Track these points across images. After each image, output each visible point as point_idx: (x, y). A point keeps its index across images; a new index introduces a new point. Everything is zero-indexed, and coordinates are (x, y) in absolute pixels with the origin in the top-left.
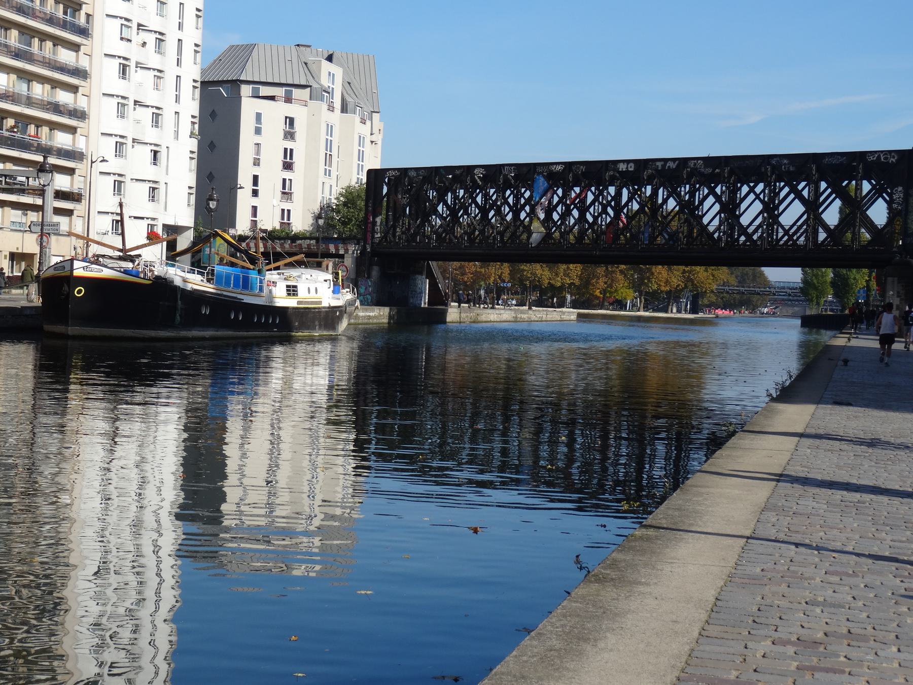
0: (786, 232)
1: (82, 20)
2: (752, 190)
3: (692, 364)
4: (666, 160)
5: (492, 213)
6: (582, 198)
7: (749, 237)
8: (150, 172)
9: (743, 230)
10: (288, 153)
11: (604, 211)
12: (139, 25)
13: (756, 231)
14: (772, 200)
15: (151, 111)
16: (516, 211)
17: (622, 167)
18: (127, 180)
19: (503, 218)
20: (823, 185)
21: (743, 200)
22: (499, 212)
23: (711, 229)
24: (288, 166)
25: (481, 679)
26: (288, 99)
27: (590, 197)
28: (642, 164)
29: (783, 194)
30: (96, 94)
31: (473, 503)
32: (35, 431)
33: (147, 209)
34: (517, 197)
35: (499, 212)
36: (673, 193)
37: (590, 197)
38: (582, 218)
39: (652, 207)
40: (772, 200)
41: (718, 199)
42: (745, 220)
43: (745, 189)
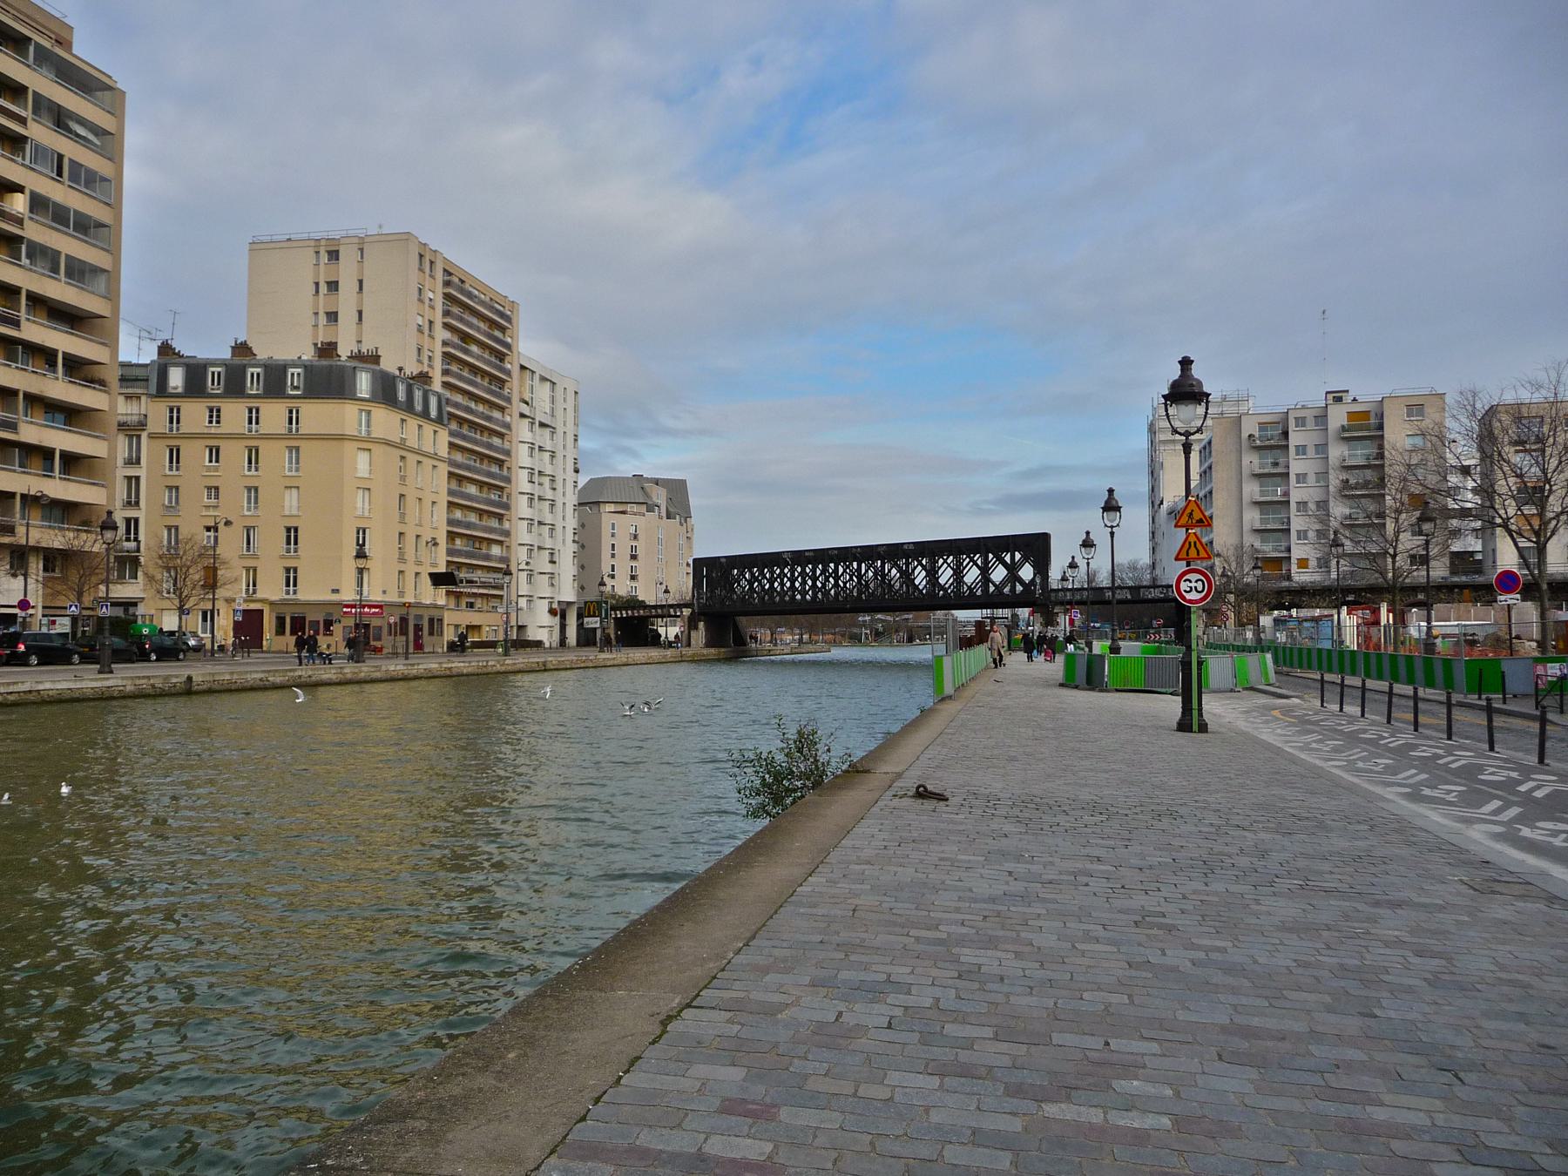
0: (969, 588)
1: (505, 472)
2: (945, 561)
5: (767, 587)
7: (945, 590)
8: (548, 568)
9: (942, 588)
11: (851, 579)
12: (540, 447)
13: (950, 587)
14: (958, 567)
16: (793, 580)
18: (535, 573)
19: (763, 587)
20: (991, 556)
21: (939, 568)
22: (760, 582)
23: (921, 587)
24: (634, 557)
27: (841, 570)
29: (965, 564)
30: (514, 519)
31: (38, 27)
34: (772, 572)
35: (760, 582)
36: (895, 565)
38: (836, 585)
40: (958, 567)
41: (924, 567)
42: (942, 581)
43: (941, 561)
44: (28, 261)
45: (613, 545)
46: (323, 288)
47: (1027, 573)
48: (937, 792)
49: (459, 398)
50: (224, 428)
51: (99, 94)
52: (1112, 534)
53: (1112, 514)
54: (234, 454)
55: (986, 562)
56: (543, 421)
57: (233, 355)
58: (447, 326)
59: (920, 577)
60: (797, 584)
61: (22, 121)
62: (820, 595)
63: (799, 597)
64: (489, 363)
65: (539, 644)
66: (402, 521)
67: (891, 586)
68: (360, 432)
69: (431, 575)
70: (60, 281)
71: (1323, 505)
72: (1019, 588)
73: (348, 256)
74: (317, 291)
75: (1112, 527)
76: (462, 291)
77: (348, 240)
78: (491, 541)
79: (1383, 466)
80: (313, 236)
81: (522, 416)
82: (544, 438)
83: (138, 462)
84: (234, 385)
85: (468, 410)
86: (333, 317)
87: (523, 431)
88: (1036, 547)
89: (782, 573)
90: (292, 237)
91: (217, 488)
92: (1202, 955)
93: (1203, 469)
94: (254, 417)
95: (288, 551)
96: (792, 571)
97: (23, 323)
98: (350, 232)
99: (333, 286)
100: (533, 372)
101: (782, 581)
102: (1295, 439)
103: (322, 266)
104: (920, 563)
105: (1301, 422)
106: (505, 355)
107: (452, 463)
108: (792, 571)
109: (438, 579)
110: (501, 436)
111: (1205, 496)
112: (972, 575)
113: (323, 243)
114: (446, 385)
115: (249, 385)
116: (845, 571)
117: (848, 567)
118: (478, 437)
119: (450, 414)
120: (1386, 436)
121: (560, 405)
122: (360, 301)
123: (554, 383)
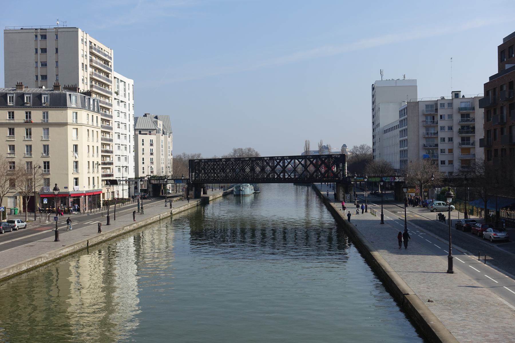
4: (278, 157)
10: (152, 150)
17: (266, 159)
24: (152, 154)
46: (39, 51)
48: (128, 194)
54: (21, 132)
56: (122, 100)
58: (91, 66)
73: (51, 37)
79: (475, 159)
81: (115, 99)
82: (121, 107)
86: (44, 64)
94: (28, 115)
95: (45, 171)
98: (51, 27)
99: (44, 51)
100: (118, 79)
102: (440, 112)
103: (39, 42)
105: (442, 105)
106: (109, 74)
113: (39, 31)
115: (43, 102)
119: (100, 106)
120: (476, 147)
123: (125, 82)
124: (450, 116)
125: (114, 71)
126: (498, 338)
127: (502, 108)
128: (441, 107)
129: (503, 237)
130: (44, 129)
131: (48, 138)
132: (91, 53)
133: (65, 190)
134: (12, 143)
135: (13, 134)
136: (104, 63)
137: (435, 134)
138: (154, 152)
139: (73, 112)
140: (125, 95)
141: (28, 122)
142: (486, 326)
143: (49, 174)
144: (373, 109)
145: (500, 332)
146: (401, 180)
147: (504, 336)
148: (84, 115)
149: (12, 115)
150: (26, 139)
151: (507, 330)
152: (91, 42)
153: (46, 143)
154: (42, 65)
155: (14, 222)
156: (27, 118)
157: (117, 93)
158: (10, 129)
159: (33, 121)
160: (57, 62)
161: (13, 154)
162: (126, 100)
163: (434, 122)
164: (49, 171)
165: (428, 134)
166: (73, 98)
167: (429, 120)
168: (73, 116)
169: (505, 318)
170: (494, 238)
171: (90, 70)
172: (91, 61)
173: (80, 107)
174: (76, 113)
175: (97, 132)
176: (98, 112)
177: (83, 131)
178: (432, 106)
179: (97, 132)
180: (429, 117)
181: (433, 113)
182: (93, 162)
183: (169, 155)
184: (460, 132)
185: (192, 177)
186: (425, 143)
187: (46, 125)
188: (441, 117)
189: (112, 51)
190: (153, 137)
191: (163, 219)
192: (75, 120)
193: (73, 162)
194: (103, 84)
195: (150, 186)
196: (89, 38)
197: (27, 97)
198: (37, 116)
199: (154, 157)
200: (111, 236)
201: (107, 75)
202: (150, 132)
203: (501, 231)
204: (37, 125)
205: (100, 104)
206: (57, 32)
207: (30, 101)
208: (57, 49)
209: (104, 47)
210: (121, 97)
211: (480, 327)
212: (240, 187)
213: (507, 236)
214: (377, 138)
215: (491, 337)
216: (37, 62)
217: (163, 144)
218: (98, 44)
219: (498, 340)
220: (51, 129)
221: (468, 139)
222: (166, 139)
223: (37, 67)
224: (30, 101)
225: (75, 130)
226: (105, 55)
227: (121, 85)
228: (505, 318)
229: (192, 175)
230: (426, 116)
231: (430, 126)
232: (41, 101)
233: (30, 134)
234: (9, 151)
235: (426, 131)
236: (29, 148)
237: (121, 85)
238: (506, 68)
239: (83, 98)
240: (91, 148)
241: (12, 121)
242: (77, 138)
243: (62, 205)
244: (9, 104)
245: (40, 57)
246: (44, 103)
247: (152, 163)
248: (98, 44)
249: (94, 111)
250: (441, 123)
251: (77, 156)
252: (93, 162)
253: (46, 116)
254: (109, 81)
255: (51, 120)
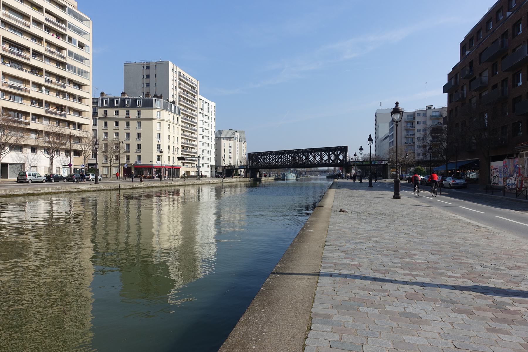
0: (325, 161)
2: (318, 154)
3: (7, 308)
4: (303, 149)
6: (281, 157)
7: (311, 162)
9: (310, 161)
10: (230, 150)
11: (285, 159)
14: (314, 156)
15: (207, 144)
16: (269, 159)
17: (295, 151)
19: (261, 161)
20: (331, 153)
25: (218, 347)
26: (230, 140)
27: (283, 157)
28: (298, 150)
32: (108, 229)
33: (208, 162)
37: (283, 157)
39: (294, 158)
41: (312, 155)
43: (310, 154)
44: (68, 70)
45: (225, 149)
46: (145, 77)
47: (341, 157)
49: (182, 108)
50: (120, 117)
51: (85, 22)
52: (370, 147)
53: (370, 142)
55: (329, 154)
57: (122, 96)
58: (180, 87)
59: (311, 158)
60: (271, 160)
61: (65, 30)
62: (277, 163)
63: (271, 164)
64: (191, 98)
65: (206, 176)
66: (169, 142)
67: (296, 161)
68: (157, 117)
69: (177, 157)
70: (76, 75)
71: (424, 137)
72: (331, 162)
73: (152, 67)
74: (143, 77)
75: (370, 145)
76: (184, 78)
77: (152, 63)
78: (192, 148)
80: (142, 62)
81: (200, 113)
82: (205, 119)
83: (96, 125)
84: (123, 104)
85: (186, 111)
86: (148, 85)
87: (200, 116)
88: (344, 150)
89: (267, 158)
90: (136, 62)
91: (107, 133)
92: (421, 240)
93: (390, 128)
94: (128, 113)
96: (269, 157)
97: (67, 87)
99: (148, 76)
100: (203, 101)
101: (268, 160)
102: (417, 119)
103: (145, 70)
104: (304, 155)
105: (419, 114)
106: (195, 96)
107: (182, 126)
108: (269, 157)
109: (179, 159)
110: (195, 118)
111: (391, 135)
112: (318, 158)
114: (180, 104)
115: (138, 104)
116: (284, 157)
117: (291, 155)
118: (188, 119)
121: (210, 110)
122: (156, 81)
124: (424, 122)
125: (200, 94)
126: (437, 263)
127: (463, 87)
128: (418, 115)
129: (462, 184)
130: (138, 123)
131: (140, 128)
132: (180, 79)
133: (151, 163)
134: (117, 131)
135: (118, 125)
136: (191, 88)
137: (413, 135)
138: (232, 151)
139: (158, 112)
140: (209, 111)
141: (128, 118)
142: (418, 240)
143: (140, 152)
144: (375, 129)
145: (446, 250)
146: (386, 163)
147: (455, 259)
148: (165, 114)
149: (117, 113)
150: (126, 129)
151: (462, 248)
152: (180, 72)
153: (139, 132)
154: (147, 86)
155: (89, 175)
156: (127, 115)
157: (202, 109)
158: (116, 122)
159: (131, 117)
160: (156, 83)
161: (117, 138)
162: (210, 115)
163: (412, 126)
164: (140, 150)
165: (408, 135)
166: (158, 102)
167: (409, 125)
168: (157, 114)
169: (460, 232)
170: (453, 184)
171: (178, 90)
172: (180, 84)
173: (163, 108)
174: (160, 112)
175: (174, 126)
176: (179, 114)
177: (165, 125)
178: (411, 116)
179: (174, 126)
180: (409, 124)
181: (412, 120)
182: (173, 147)
183: (243, 155)
184: (431, 133)
185: (249, 164)
186: (406, 141)
187: (139, 120)
188: (418, 123)
189: (198, 82)
190: (232, 142)
191: (213, 183)
192: (158, 117)
193: (157, 145)
194: (190, 101)
195: (225, 170)
196: (178, 70)
197: (127, 101)
198: (133, 113)
199: (232, 154)
200: (151, 186)
201: (194, 96)
202: (230, 139)
203: (459, 178)
204: (133, 119)
205: (181, 111)
206: (156, 65)
207: (129, 104)
208: (156, 75)
209: (191, 78)
210: (205, 112)
211: (403, 241)
212: (285, 174)
213: (466, 183)
214: (377, 147)
215: (418, 259)
216: (143, 84)
217: (239, 147)
218: (186, 75)
219: (436, 266)
220: (142, 122)
221: (437, 137)
222: (241, 145)
223: (143, 87)
224: (129, 104)
225: (159, 123)
226: (192, 83)
227: (206, 105)
228: (460, 232)
229: (249, 163)
230: (407, 122)
231: (410, 130)
232: (136, 104)
233: (129, 126)
234: (115, 137)
235: (407, 132)
236: (128, 134)
237: (206, 105)
238: (467, 54)
239: (166, 103)
240: (172, 138)
241: (117, 117)
242: (160, 129)
243: (149, 173)
244: (115, 106)
245: (146, 81)
246: (138, 105)
247: (230, 158)
248: (186, 75)
249: (175, 113)
250: (417, 127)
251: (159, 141)
252: (173, 147)
253: (139, 113)
254: (195, 100)
255: (142, 116)
